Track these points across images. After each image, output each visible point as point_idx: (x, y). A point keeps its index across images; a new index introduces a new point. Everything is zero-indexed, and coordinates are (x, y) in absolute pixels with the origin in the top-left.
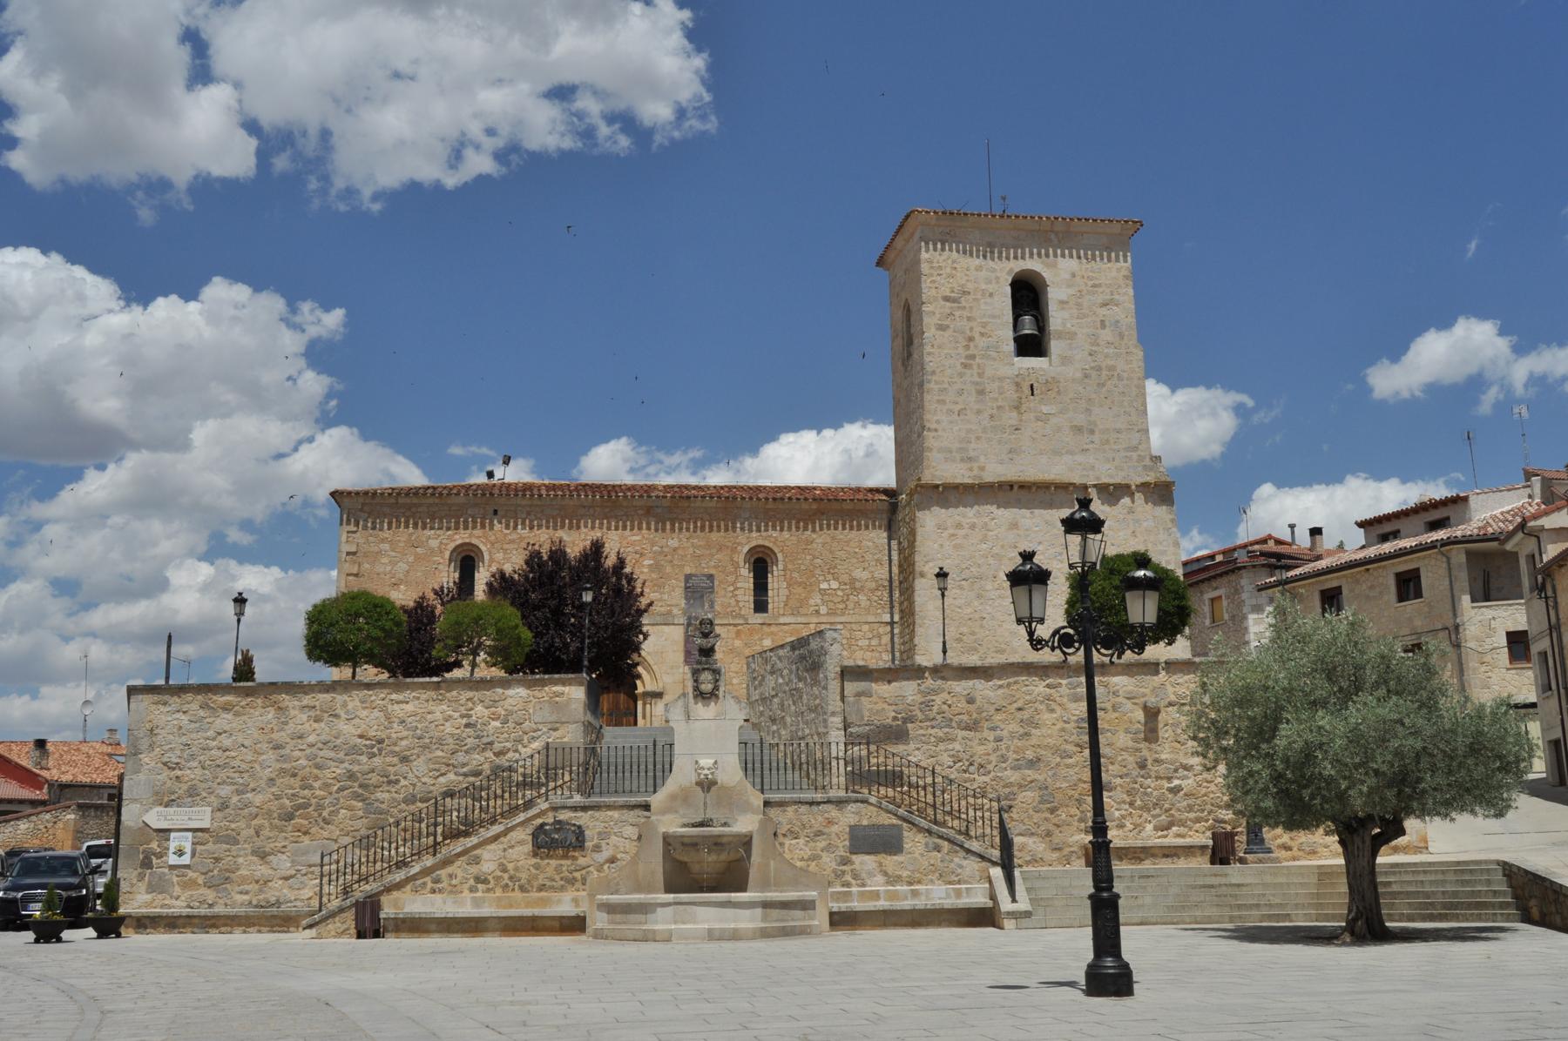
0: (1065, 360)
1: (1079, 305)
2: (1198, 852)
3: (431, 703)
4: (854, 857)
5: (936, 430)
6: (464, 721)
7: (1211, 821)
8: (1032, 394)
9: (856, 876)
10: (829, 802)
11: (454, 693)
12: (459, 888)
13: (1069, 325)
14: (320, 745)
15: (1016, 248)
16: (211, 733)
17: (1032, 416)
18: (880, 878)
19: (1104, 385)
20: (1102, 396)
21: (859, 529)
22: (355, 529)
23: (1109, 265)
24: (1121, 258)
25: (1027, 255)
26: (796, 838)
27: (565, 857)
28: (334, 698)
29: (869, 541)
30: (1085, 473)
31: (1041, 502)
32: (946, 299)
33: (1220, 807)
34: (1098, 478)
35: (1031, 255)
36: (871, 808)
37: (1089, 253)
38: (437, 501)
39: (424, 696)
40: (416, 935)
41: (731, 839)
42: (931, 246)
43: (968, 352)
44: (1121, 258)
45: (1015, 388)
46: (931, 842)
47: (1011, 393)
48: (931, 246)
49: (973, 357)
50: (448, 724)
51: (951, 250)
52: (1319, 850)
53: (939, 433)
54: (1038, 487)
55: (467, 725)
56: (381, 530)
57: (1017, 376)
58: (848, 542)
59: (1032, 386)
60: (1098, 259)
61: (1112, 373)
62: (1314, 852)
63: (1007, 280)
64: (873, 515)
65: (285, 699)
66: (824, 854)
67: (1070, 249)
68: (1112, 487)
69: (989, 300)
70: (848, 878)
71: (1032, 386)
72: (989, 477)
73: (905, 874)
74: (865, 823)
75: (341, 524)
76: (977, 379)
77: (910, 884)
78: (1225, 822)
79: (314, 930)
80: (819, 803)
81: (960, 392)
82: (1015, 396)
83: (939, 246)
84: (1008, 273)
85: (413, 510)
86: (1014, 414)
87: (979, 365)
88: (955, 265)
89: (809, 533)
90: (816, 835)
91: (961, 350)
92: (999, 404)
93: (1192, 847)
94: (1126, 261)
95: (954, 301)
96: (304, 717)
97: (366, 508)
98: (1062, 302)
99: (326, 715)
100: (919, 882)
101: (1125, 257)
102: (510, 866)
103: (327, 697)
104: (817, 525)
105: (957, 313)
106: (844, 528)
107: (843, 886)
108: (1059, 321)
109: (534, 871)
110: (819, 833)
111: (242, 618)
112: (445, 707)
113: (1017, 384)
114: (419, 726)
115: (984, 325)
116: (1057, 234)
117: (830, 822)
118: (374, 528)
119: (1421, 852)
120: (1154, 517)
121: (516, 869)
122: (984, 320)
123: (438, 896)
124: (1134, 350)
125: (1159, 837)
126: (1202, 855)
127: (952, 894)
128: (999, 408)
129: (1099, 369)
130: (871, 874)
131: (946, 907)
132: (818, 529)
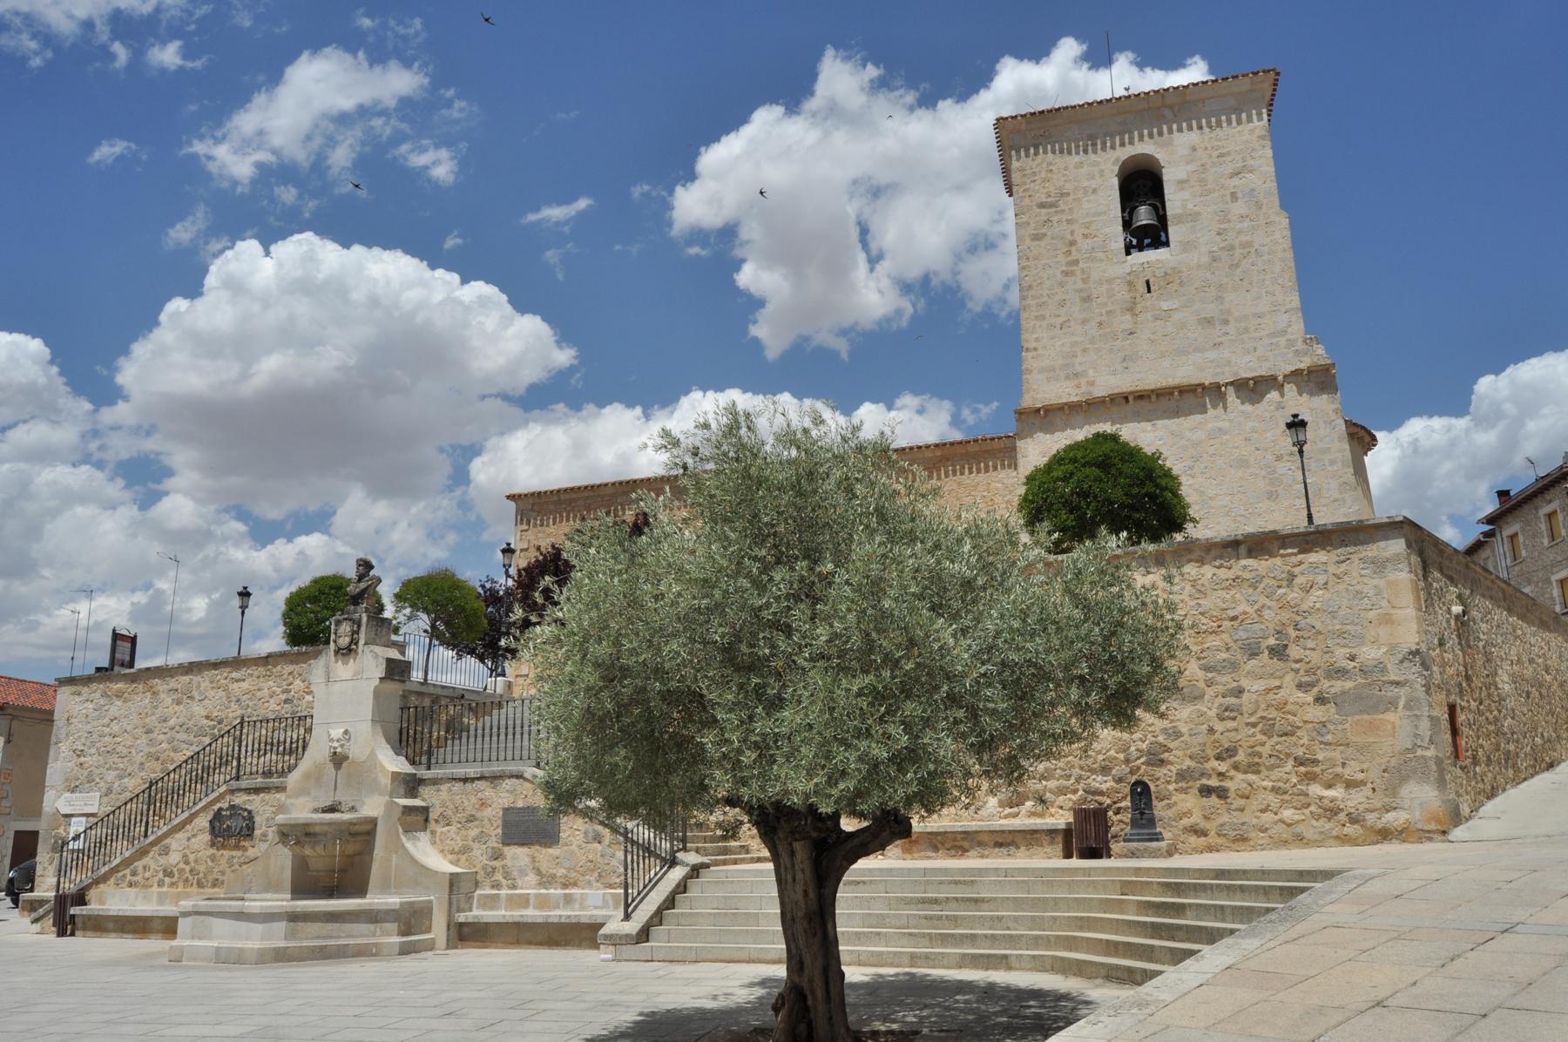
0: (1187, 246)
1: (1202, 182)
2: (1046, 839)
3: (261, 679)
4: (506, 849)
5: (1035, 349)
6: (284, 697)
7: (1081, 792)
8: (1149, 291)
9: (507, 875)
10: (482, 778)
11: (279, 667)
12: (150, 882)
13: (1190, 206)
14: (177, 728)
15: (1122, 134)
16: (106, 721)
17: (1149, 316)
18: (532, 878)
19: (1237, 266)
20: (1237, 279)
21: (987, 471)
22: (527, 527)
23: (1240, 128)
24: (1255, 117)
25: (1136, 139)
26: (448, 825)
27: (237, 847)
28: (191, 680)
29: (999, 482)
30: (1220, 370)
31: (1165, 412)
32: (1042, 205)
33: (1093, 771)
34: (1235, 374)
35: (1141, 138)
36: (527, 785)
37: (1213, 120)
38: (591, 493)
39: (256, 673)
40: (98, 934)
41: (326, 828)
42: (1023, 153)
43: (1069, 259)
44: (1255, 117)
45: (1126, 288)
46: (590, 830)
47: (1123, 294)
48: (1023, 153)
49: (1076, 262)
50: (272, 701)
51: (1045, 152)
52: (1252, 835)
53: (1040, 352)
54: (1158, 395)
55: (286, 701)
56: (547, 526)
57: (1129, 274)
58: (975, 487)
59: (1148, 282)
60: (1225, 124)
61: (1247, 250)
62: (1243, 839)
63: (1112, 171)
64: (1001, 455)
65: (159, 684)
66: (476, 846)
67: (1189, 121)
68: (1251, 382)
69: (1093, 197)
70: (498, 876)
71: (1148, 282)
72: (1100, 391)
73: (561, 872)
74: (520, 804)
75: (516, 524)
76: (1080, 285)
77: (565, 886)
78: (1101, 793)
79: (39, 924)
80: (473, 780)
81: (1062, 303)
82: (1128, 297)
83: (1032, 151)
84: (1114, 164)
85: (573, 504)
86: (1128, 317)
87: (1083, 271)
88: (1051, 167)
89: (934, 481)
90: (469, 821)
91: (1061, 258)
92: (1109, 309)
93: (1035, 832)
94: (1260, 119)
95: (1052, 205)
96: (169, 700)
97: (536, 508)
98: (1181, 182)
99: (185, 697)
100: (575, 884)
101: (1259, 115)
102: (192, 857)
103: (186, 679)
104: (943, 472)
105: (1055, 219)
106: (971, 472)
107: (493, 887)
108: (1178, 204)
109: (210, 863)
110: (472, 819)
111: (246, 611)
112: (271, 683)
113: (1130, 283)
114: (251, 704)
115: (1087, 225)
116: (1171, 107)
117: (483, 804)
118: (542, 525)
119: (1430, 839)
120: (1312, 410)
121: (196, 861)
122: (1088, 220)
123: (133, 891)
124: (1277, 219)
125: (1006, 817)
126: (1052, 843)
127: (611, 903)
128: (1109, 313)
129: (1231, 248)
130: (523, 873)
131: (583, 920)
132: (943, 476)
